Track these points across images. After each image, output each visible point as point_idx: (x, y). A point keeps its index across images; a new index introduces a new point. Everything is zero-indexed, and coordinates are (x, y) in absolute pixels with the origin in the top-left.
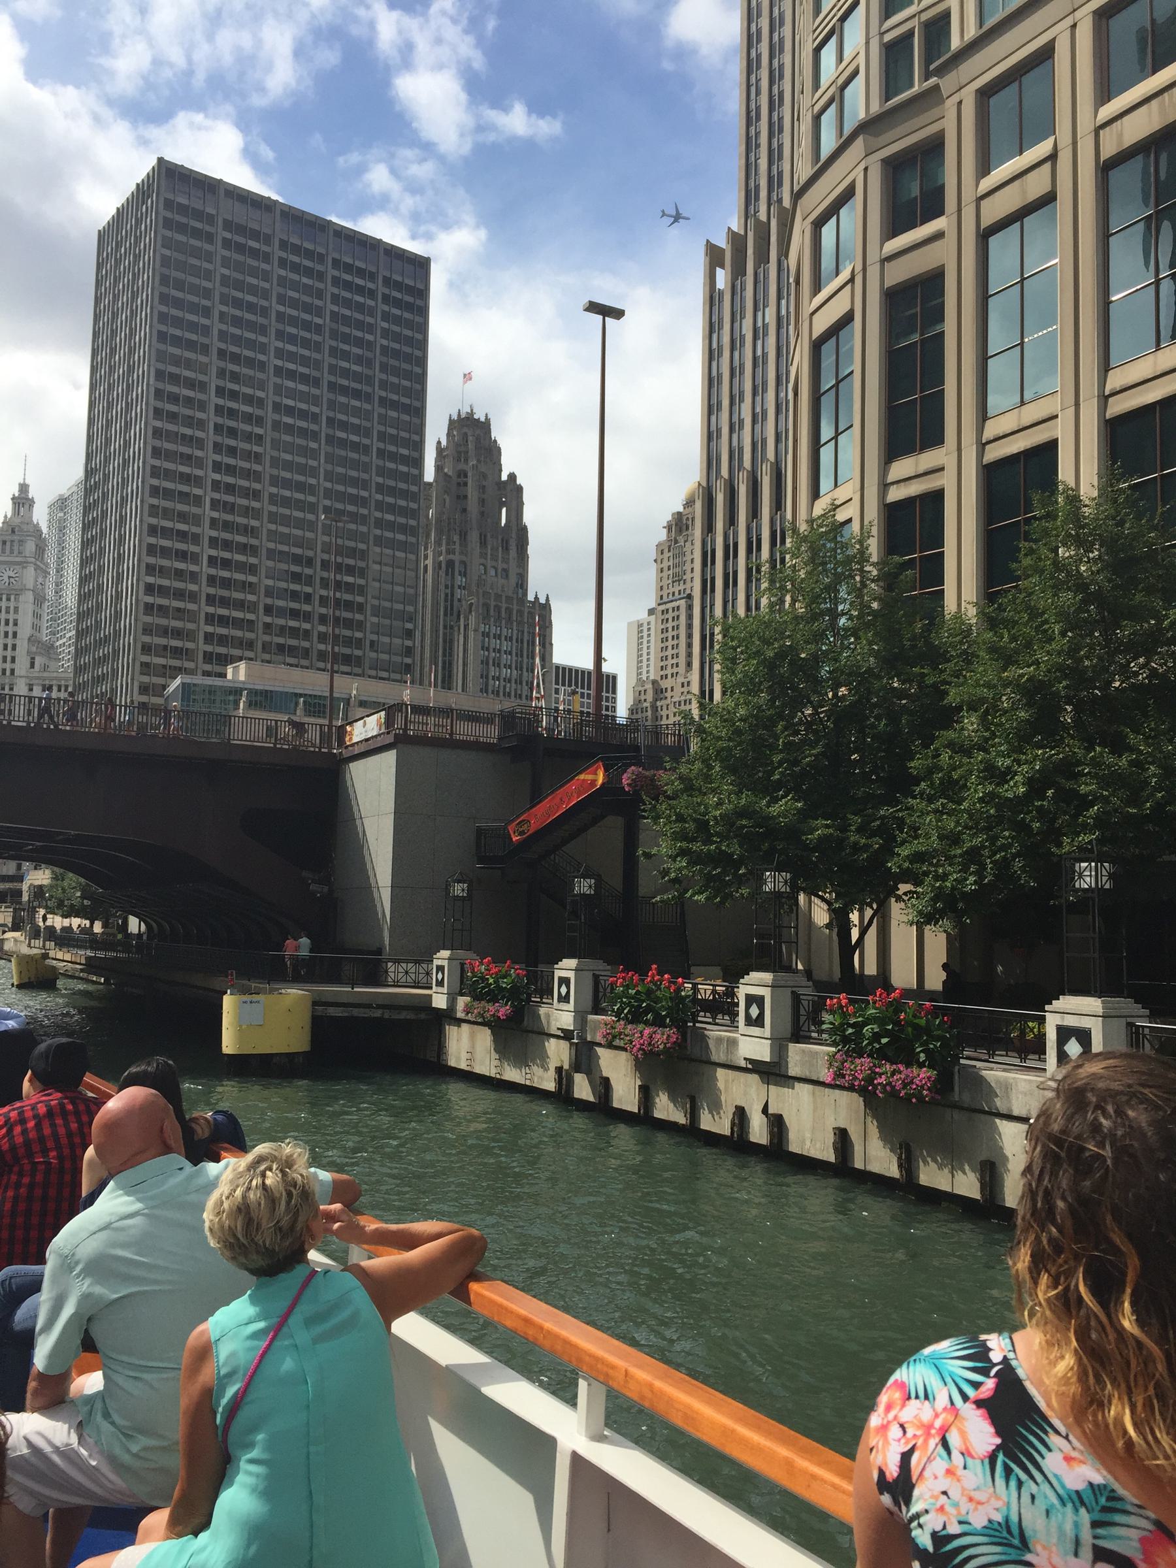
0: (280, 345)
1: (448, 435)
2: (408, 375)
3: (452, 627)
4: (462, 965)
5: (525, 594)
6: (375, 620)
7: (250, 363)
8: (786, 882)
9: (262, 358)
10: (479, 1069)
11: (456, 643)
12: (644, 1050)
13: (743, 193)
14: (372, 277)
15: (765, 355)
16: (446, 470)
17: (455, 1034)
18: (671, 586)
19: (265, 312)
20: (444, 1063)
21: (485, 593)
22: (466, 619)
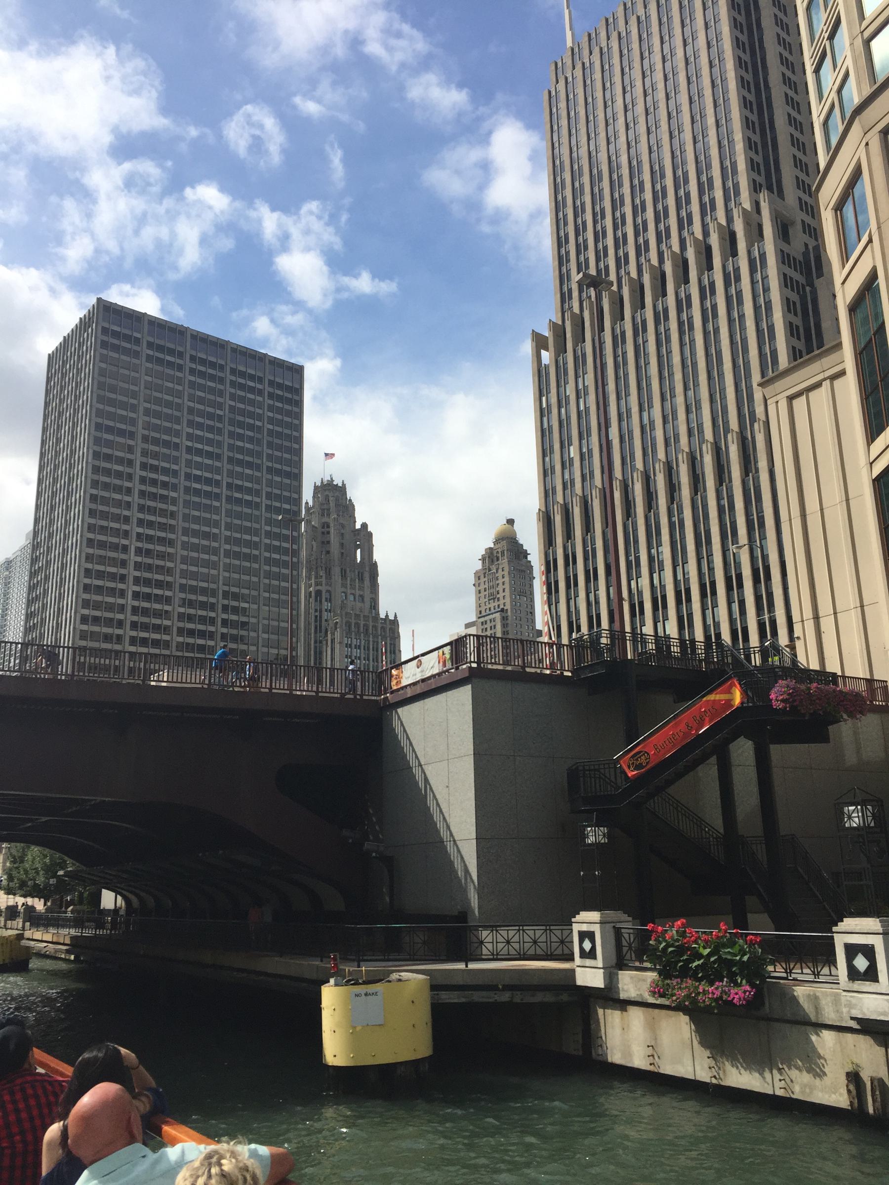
0: (190, 430)
1: (314, 497)
2: (289, 450)
3: (321, 642)
6: (266, 636)
7: (167, 444)
8: (604, 835)
9: (177, 440)
10: (668, 1068)
11: (325, 654)
13: (559, 295)
14: (260, 380)
15: (550, 427)
16: (313, 523)
18: (487, 603)
19: (179, 407)
20: (600, 1058)
21: (347, 614)
22: (333, 634)
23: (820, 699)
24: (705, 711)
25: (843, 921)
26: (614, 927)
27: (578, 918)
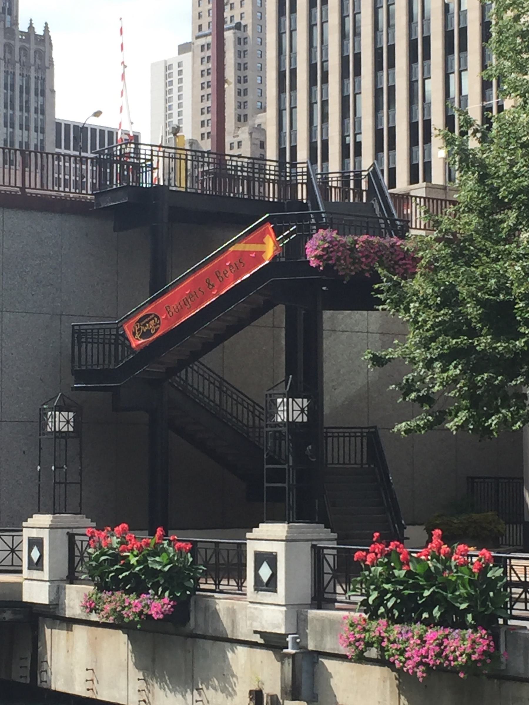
4: (71, 537)
5: (15, 22)
12: (426, 664)
17: (63, 643)
20: (44, 686)
23: (367, 257)
24: (230, 265)
25: (258, 527)
26: (68, 533)
27: (31, 522)
